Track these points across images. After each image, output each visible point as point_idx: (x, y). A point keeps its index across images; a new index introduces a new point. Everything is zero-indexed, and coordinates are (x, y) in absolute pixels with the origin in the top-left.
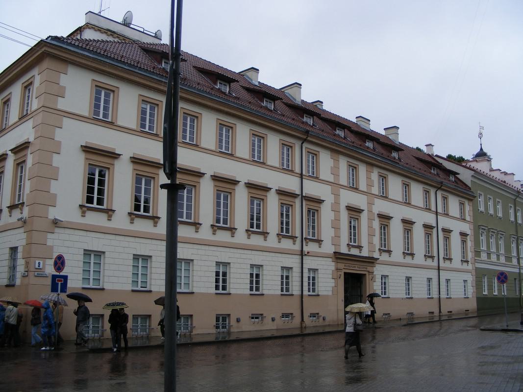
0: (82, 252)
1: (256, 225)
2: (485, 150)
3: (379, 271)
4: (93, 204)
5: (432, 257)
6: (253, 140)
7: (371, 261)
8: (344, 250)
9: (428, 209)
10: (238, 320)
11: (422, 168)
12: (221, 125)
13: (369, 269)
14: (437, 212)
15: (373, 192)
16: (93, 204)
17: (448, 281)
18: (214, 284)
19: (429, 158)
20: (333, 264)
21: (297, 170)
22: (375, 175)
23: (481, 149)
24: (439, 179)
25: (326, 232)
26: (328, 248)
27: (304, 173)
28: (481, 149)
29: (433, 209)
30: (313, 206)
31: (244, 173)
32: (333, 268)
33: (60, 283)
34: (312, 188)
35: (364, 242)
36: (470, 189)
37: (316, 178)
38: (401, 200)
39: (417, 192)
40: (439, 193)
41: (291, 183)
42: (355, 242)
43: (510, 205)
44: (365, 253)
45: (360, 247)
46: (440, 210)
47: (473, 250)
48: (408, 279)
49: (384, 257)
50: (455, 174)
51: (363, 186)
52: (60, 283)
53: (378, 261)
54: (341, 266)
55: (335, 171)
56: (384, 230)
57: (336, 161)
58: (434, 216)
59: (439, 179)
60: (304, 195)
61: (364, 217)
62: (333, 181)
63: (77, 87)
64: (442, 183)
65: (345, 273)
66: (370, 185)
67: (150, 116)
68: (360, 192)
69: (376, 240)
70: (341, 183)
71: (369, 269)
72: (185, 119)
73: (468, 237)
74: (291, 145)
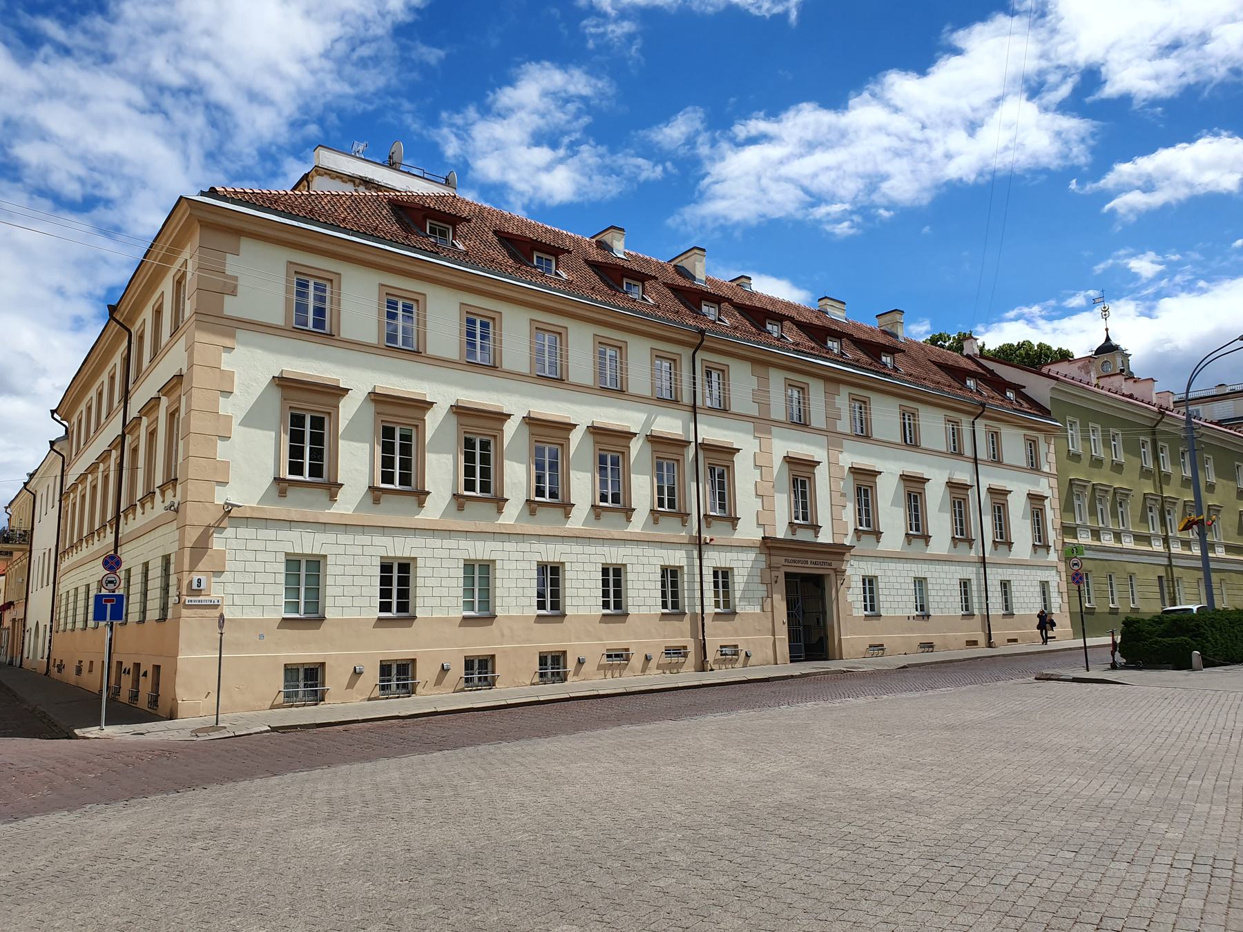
0: (282, 558)
1: (614, 501)
2: (1114, 341)
3: (855, 571)
4: (301, 474)
5: (970, 542)
6: (600, 352)
7: (838, 551)
8: (781, 532)
9: (957, 452)
10: (580, 662)
11: (942, 381)
12: (602, 343)
13: (835, 565)
14: (976, 459)
15: (839, 430)
16: (301, 474)
17: (1005, 585)
18: (660, 601)
19: (969, 361)
20: (763, 557)
21: (686, 399)
22: (843, 400)
23: (1108, 339)
24: (978, 398)
25: (746, 502)
26: (749, 531)
27: (699, 403)
28: (1108, 339)
29: (968, 451)
30: (718, 459)
31: (584, 413)
32: (763, 565)
33: (109, 605)
34: (712, 432)
35: (823, 516)
36: (1048, 412)
37: (723, 409)
38: (944, 450)
39: (933, 426)
40: (981, 425)
41: (670, 424)
42: (868, 525)
43: (1142, 438)
44: (825, 537)
45: (816, 528)
46: (982, 454)
47: (1058, 526)
48: (920, 582)
49: (867, 542)
50: (1017, 388)
51: (818, 418)
52: (109, 605)
53: (853, 552)
54: (779, 560)
55: (761, 397)
56: (960, 507)
57: (763, 380)
58: (971, 466)
59: (978, 398)
60: (699, 441)
61: (972, 494)
62: (757, 414)
63: (261, 280)
64: (983, 405)
65: (787, 575)
66: (832, 417)
67: (483, 338)
68: (341, 344)
69: (849, 514)
70: (773, 417)
71: (835, 565)
72: (709, 374)
73: (1047, 502)
74: (559, 330)
